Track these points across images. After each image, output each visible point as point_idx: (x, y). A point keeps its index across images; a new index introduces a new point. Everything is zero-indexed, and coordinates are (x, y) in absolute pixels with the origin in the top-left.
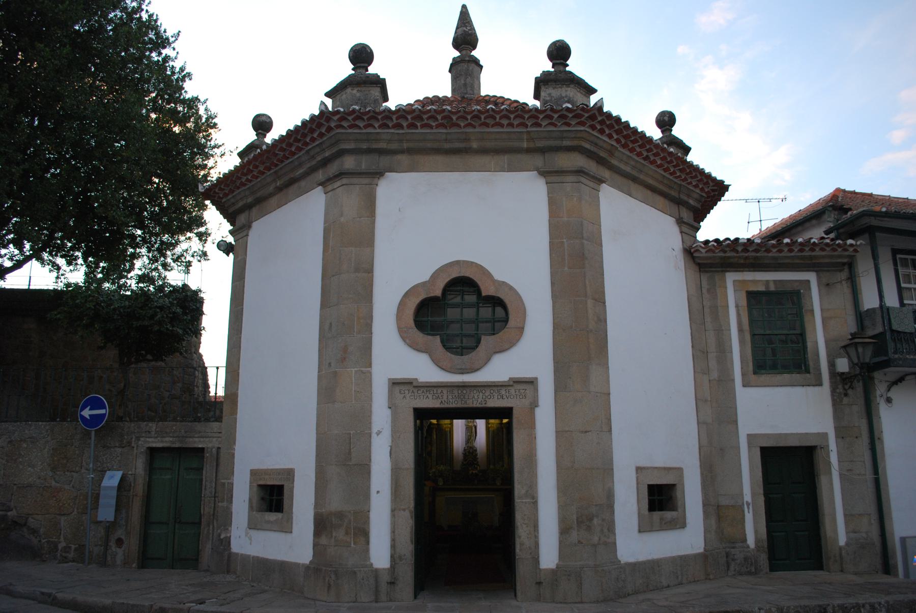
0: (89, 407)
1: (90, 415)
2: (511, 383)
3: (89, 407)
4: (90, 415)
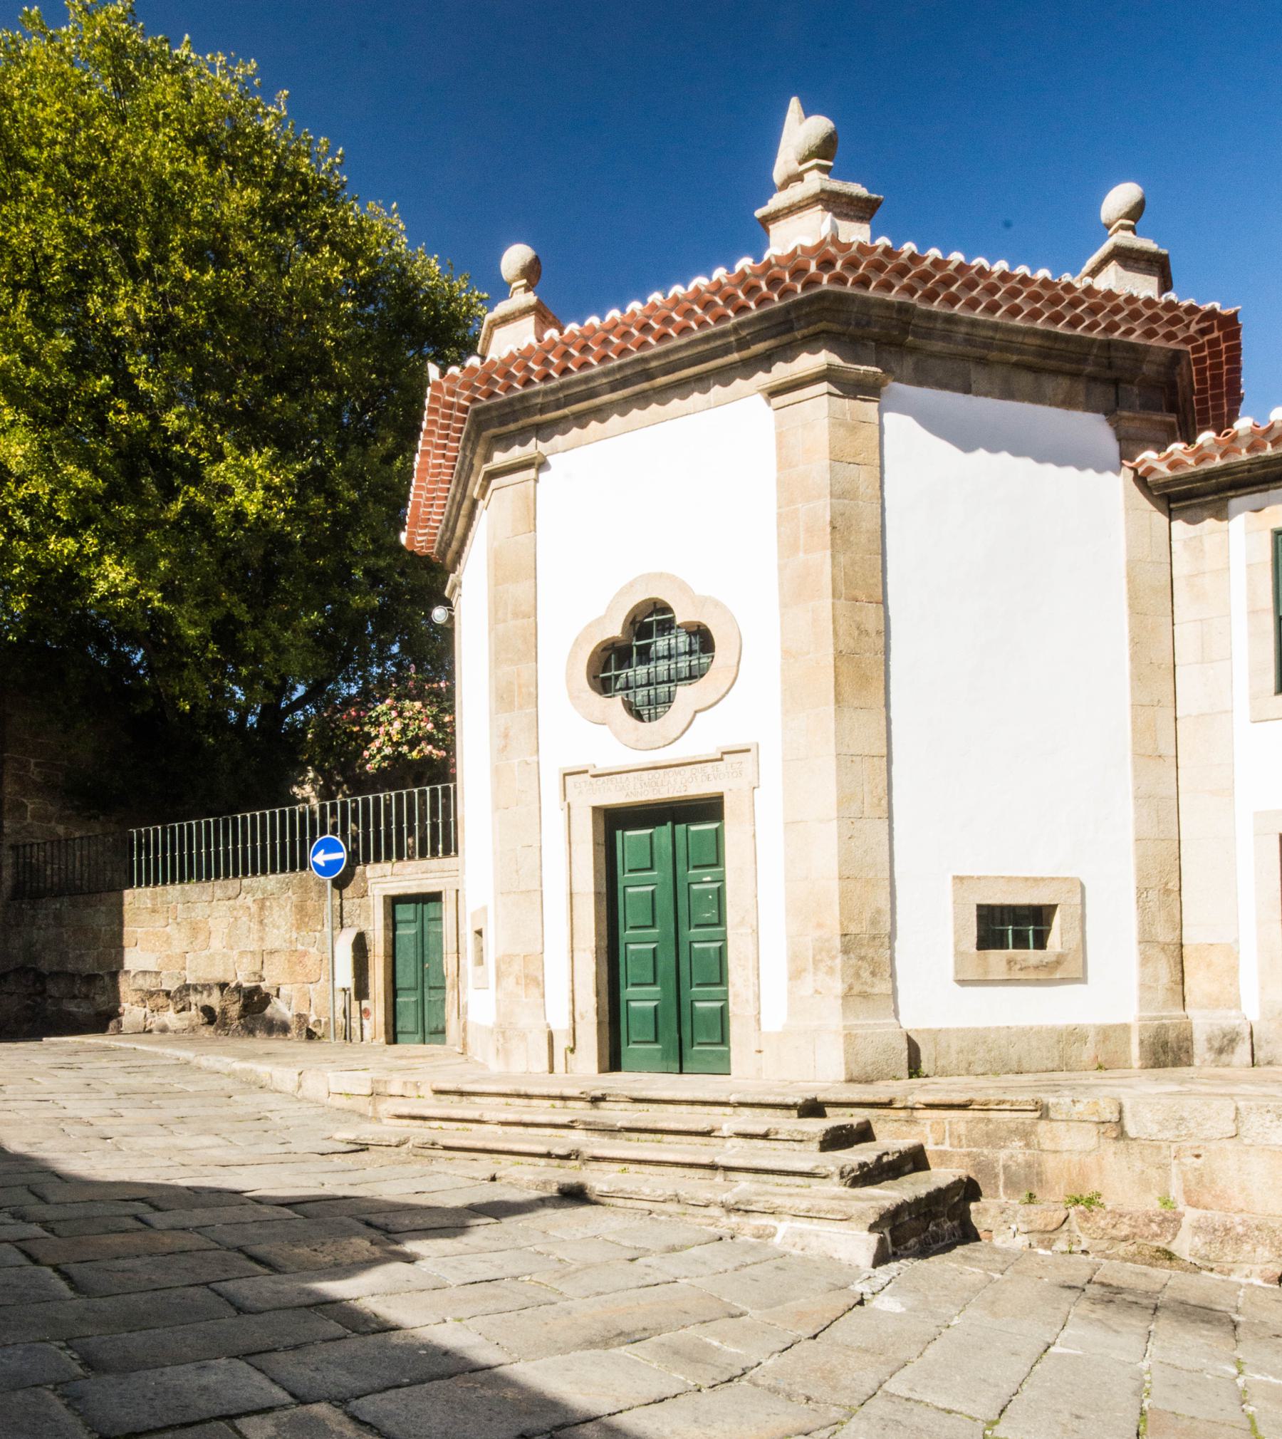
0: (323, 851)
1: (325, 862)
3: (323, 851)
4: (325, 862)
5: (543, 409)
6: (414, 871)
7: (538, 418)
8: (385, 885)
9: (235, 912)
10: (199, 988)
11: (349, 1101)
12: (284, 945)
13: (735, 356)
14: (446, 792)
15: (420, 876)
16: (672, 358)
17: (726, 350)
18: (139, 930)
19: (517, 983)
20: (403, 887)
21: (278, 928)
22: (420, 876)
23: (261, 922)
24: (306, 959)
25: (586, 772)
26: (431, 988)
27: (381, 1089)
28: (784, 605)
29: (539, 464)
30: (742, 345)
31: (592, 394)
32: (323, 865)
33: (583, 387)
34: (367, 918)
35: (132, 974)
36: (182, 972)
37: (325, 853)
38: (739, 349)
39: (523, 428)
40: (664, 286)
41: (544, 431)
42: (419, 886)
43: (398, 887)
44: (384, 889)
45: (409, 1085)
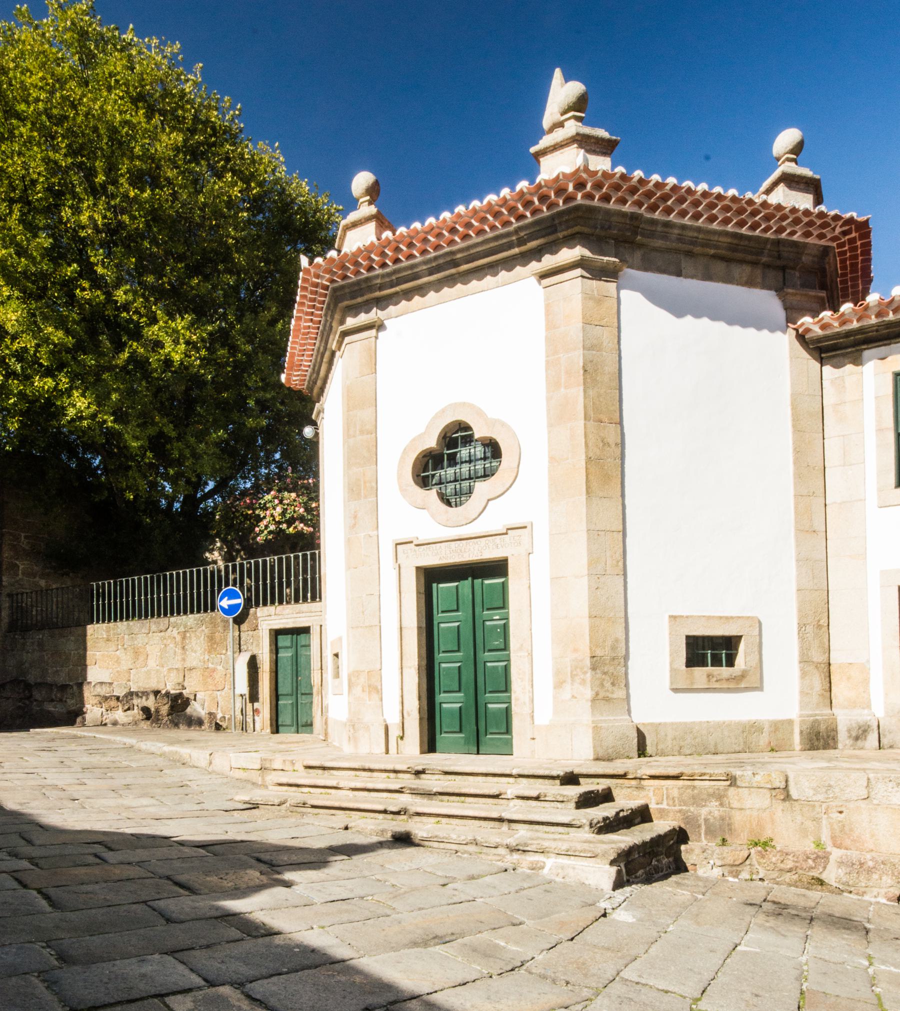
2: (399, 562)
3: (226, 598)
4: (229, 606)
5: (381, 288)
6: (291, 612)
7: (378, 294)
8: (270, 622)
9: (165, 641)
10: (140, 694)
11: (245, 774)
12: (199, 664)
13: (516, 250)
14: (313, 556)
15: (295, 615)
16: (472, 251)
17: (510, 246)
18: (98, 653)
19: (363, 691)
20: (283, 623)
21: (195, 652)
22: (295, 615)
23: (183, 648)
24: (215, 674)
25: (417, 545)
26: (302, 694)
27: (267, 765)
28: (550, 425)
29: (379, 326)
30: (521, 242)
31: (416, 277)
32: (227, 607)
33: (410, 272)
34: (258, 645)
35: (93, 684)
36: (128, 683)
37: (228, 599)
38: (519, 245)
39: (367, 301)
40: (466, 201)
41: (382, 303)
42: (294, 622)
43: (279, 624)
44: (269, 625)
45: (287, 763)
